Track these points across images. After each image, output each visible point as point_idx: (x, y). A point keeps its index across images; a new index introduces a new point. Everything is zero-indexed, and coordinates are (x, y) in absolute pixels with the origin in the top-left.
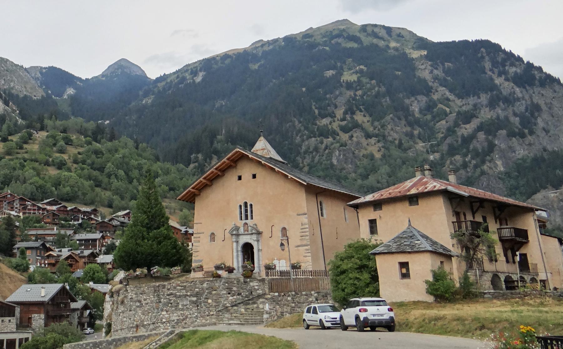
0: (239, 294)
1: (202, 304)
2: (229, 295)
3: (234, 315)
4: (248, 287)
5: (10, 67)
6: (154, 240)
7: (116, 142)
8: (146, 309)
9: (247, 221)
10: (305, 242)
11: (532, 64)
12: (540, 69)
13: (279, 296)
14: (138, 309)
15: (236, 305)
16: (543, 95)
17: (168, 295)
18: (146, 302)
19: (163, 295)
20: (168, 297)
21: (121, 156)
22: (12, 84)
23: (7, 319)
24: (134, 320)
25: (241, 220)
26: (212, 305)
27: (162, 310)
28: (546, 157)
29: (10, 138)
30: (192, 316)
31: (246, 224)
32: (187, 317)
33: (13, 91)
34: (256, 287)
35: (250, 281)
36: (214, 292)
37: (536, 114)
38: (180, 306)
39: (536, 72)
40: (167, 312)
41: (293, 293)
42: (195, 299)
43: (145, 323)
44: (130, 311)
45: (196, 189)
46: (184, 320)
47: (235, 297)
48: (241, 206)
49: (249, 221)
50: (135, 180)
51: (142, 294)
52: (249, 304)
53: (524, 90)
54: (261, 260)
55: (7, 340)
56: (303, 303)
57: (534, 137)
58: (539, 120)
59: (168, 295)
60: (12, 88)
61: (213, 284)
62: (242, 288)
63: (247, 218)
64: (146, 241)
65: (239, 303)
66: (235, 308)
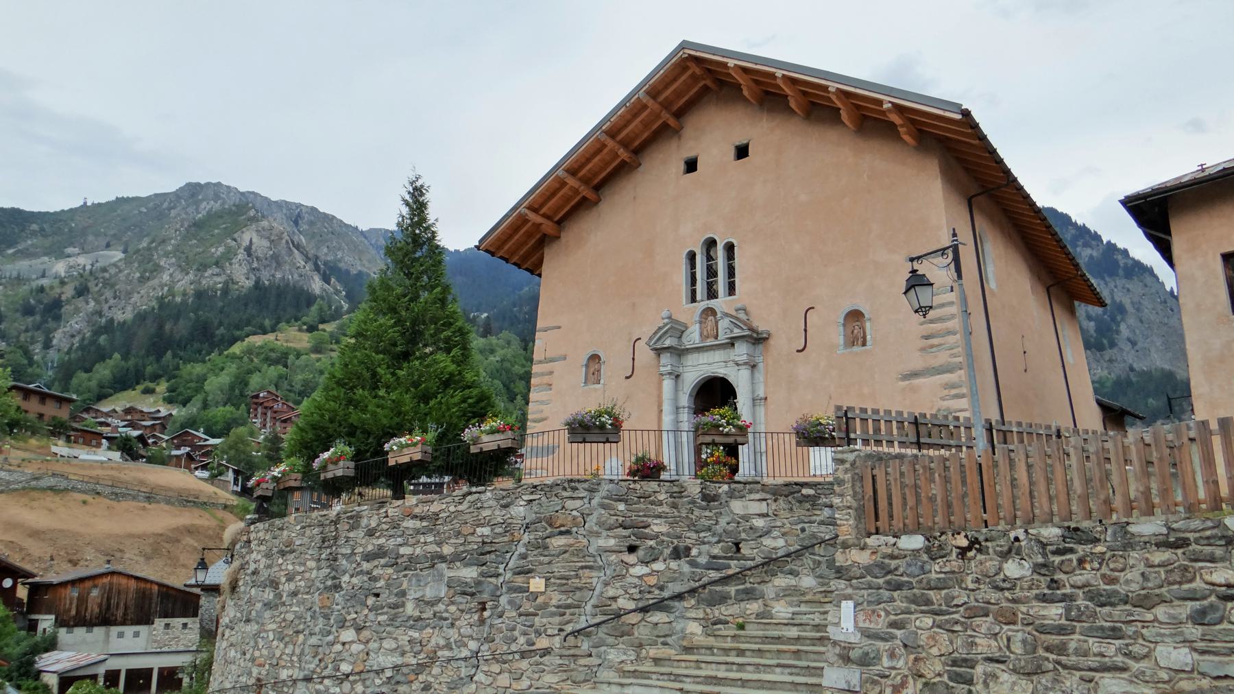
0: (677, 554)
1: (503, 600)
2: (631, 558)
3: (653, 652)
4: (723, 521)
5: (338, 229)
6: (407, 391)
7: (493, 339)
8: (290, 617)
9: (712, 303)
10: (942, 358)
11: (1115, 245)
12: (1125, 252)
13: (934, 552)
14: (267, 614)
15: (660, 605)
16: (1128, 290)
17: (368, 557)
18: (292, 586)
19: (348, 557)
20: (366, 566)
21: (498, 358)
22: (340, 254)
23: (177, 622)
24: (253, 660)
25: (693, 300)
26: (545, 606)
27: (342, 624)
28: (1134, 379)
29: (321, 326)
30: (456, 653)
31: (710, 311)
32: (433, 658)
33: (341, 265)
34: (759, 523)
35: (732, 495)
36: (558, 542)
37: (1119, 318)
38: (410, 609)
39: (1120, 257)
40: (359, 629)
41: (1051, 533)
42: (469, 573)
43: (284, 674)
44: (248, 621)
45: (544, 216)
46: (421, 668)
47: (659, 566)
48: (692, 257)
49: (722, 303)
50: (519, 397)
51: (283, 553)
52: (723, 599)
53: (1102, 282)
54: (770, 407)
55: (161, 670)
56: (1146, 602)
57: (1115, 350)
58: (1123, 327)
59: (368, 557)
60: (340, 261)
61: (556, 503)
62: (692, 526)
63: (712, 294)
64: (382, 393)
65: (679, 597)
66: (658, 617)
